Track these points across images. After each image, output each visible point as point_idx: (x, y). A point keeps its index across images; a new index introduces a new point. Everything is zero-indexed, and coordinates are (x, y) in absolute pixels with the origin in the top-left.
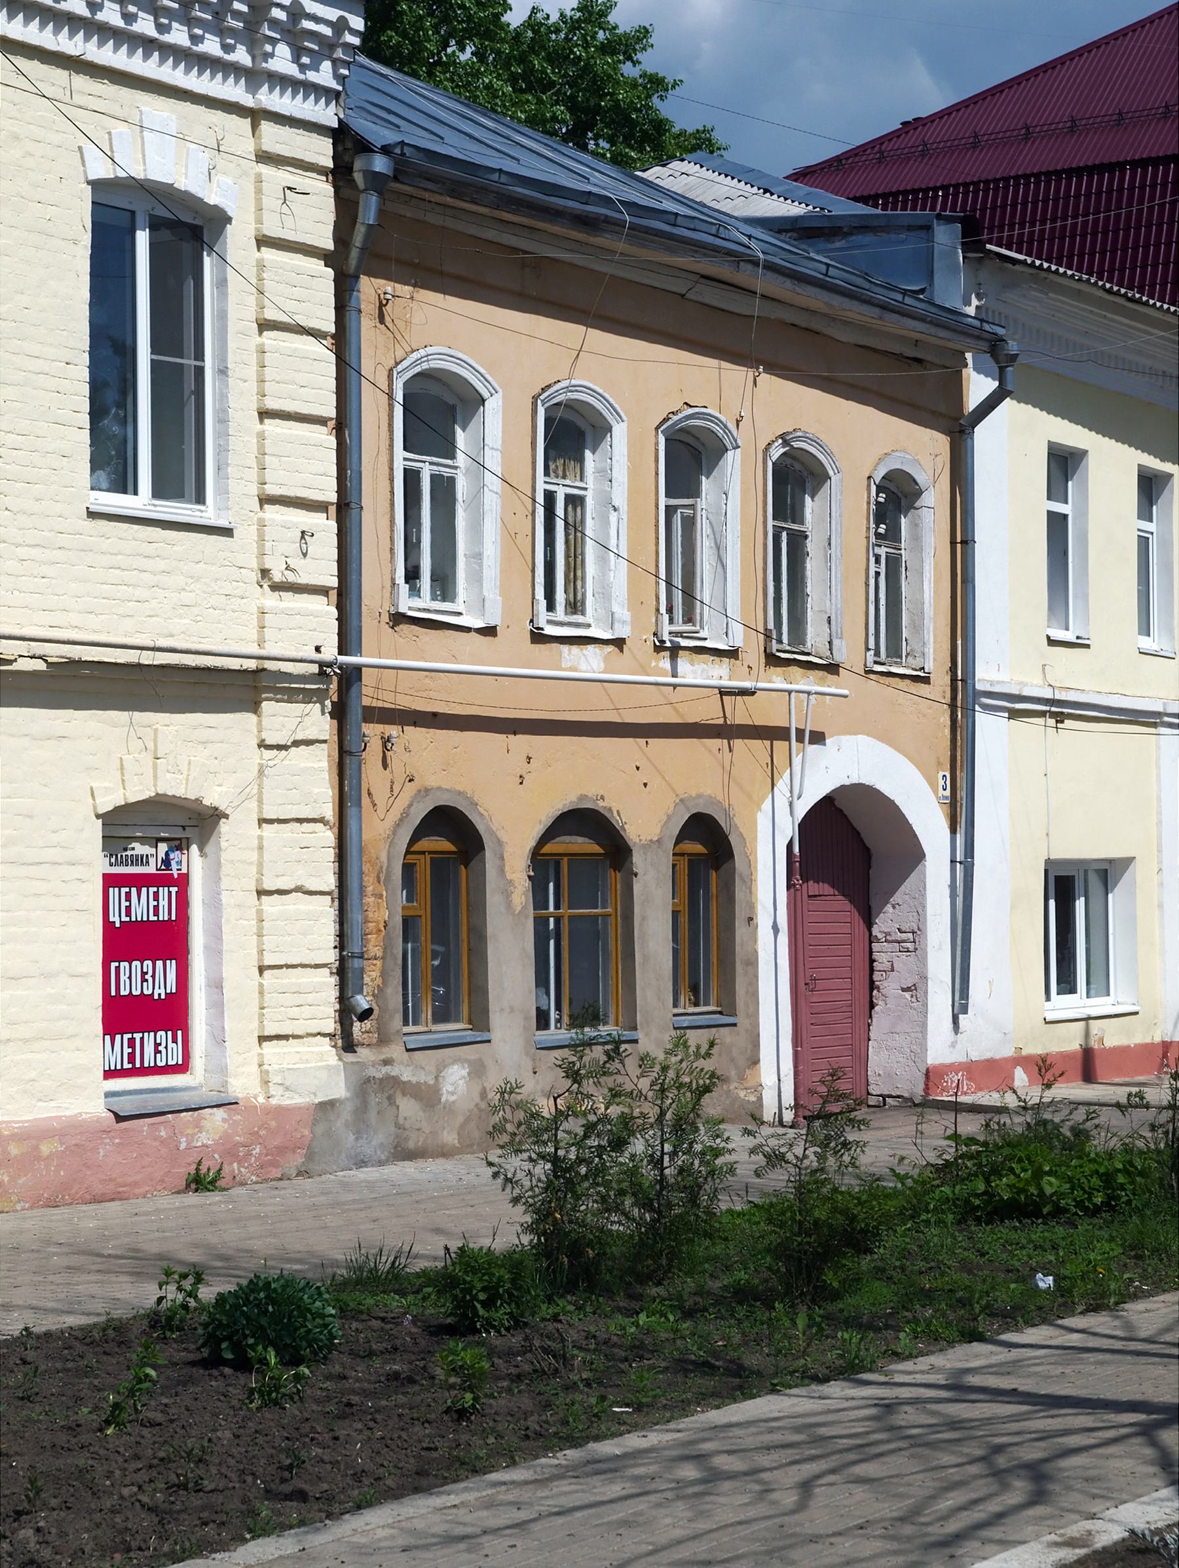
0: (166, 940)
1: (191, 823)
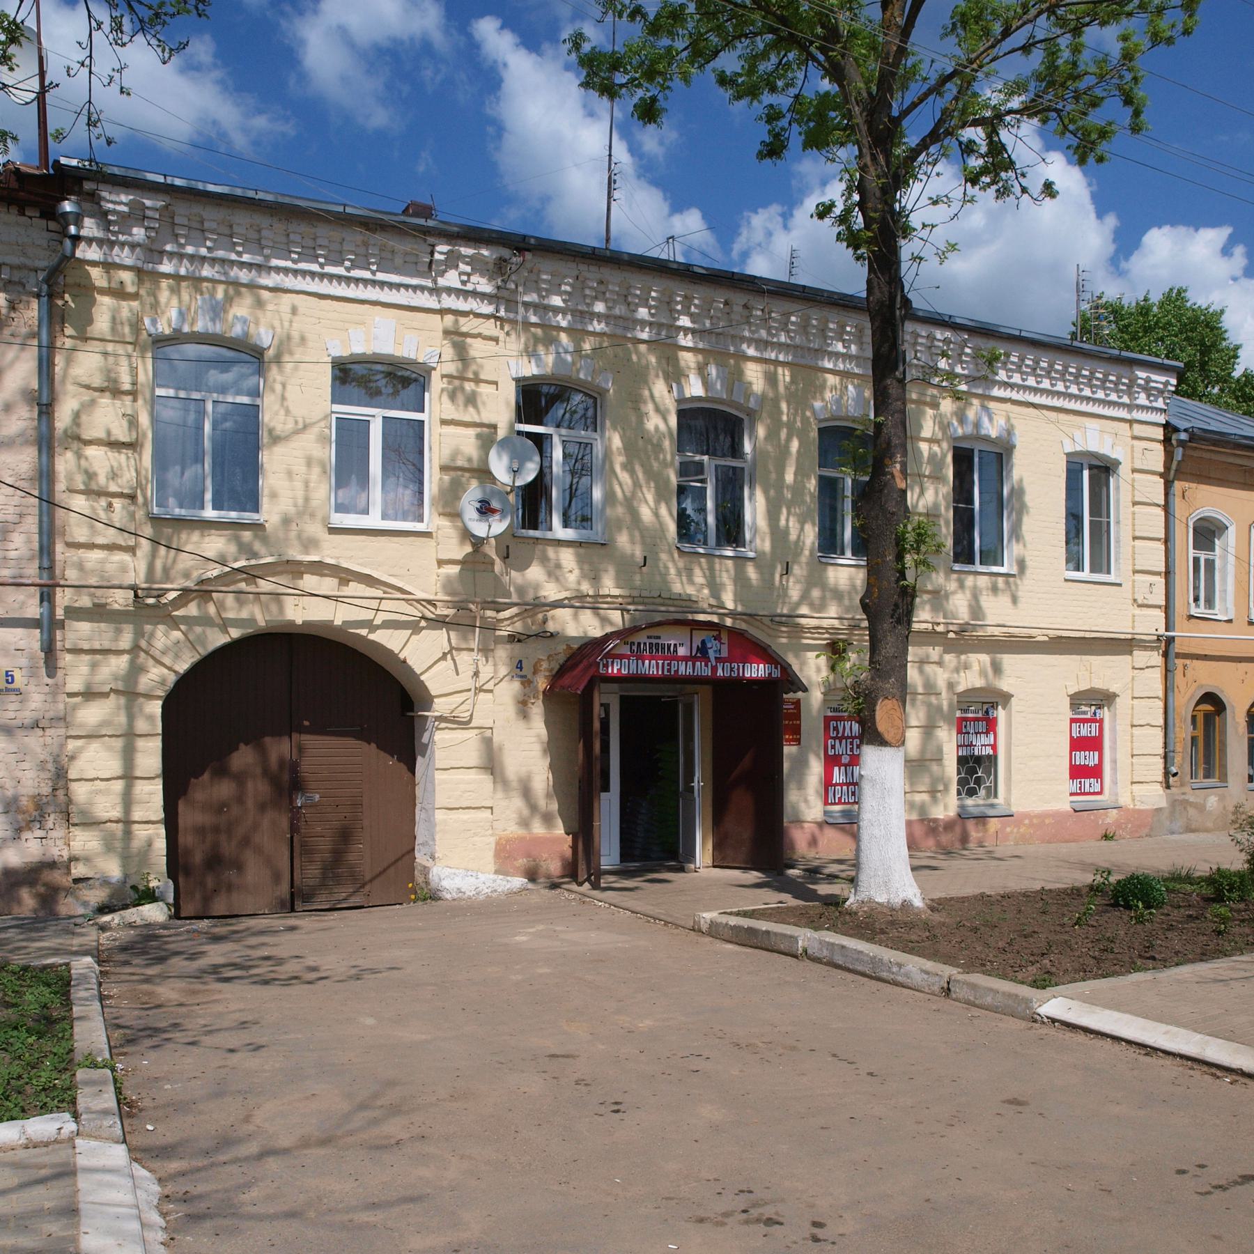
0: (1094, 744)
1: (1104, 699)
